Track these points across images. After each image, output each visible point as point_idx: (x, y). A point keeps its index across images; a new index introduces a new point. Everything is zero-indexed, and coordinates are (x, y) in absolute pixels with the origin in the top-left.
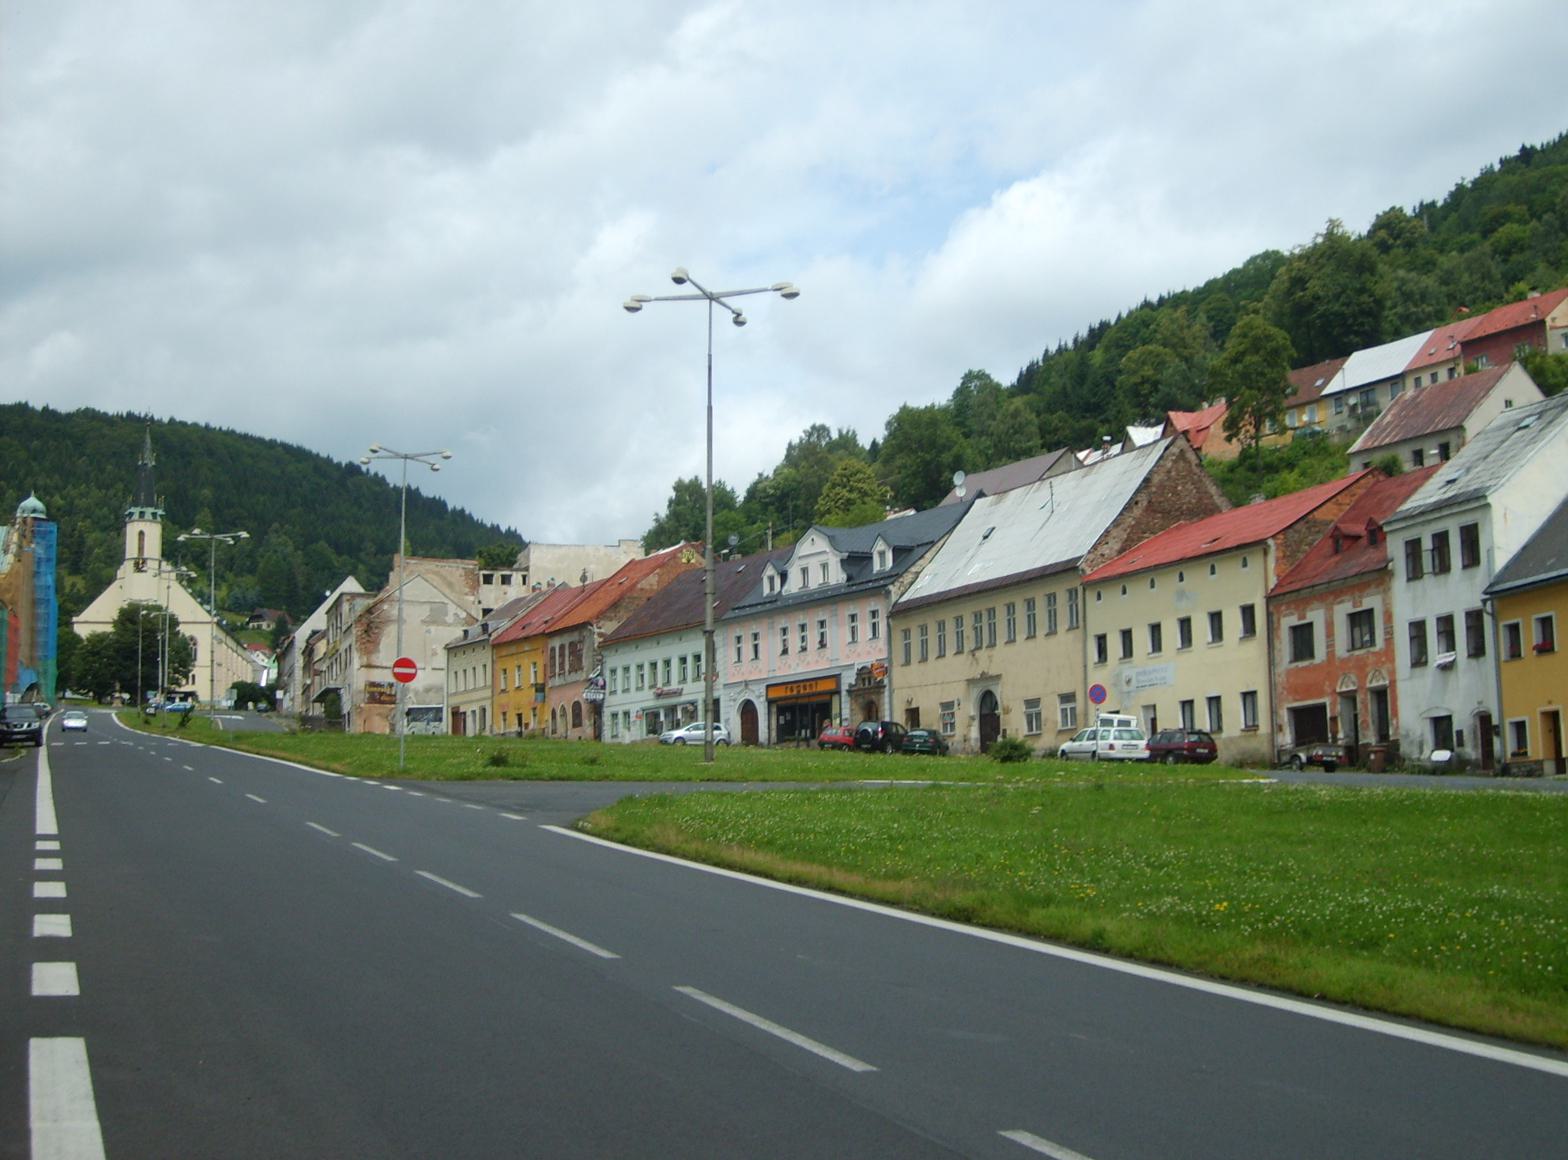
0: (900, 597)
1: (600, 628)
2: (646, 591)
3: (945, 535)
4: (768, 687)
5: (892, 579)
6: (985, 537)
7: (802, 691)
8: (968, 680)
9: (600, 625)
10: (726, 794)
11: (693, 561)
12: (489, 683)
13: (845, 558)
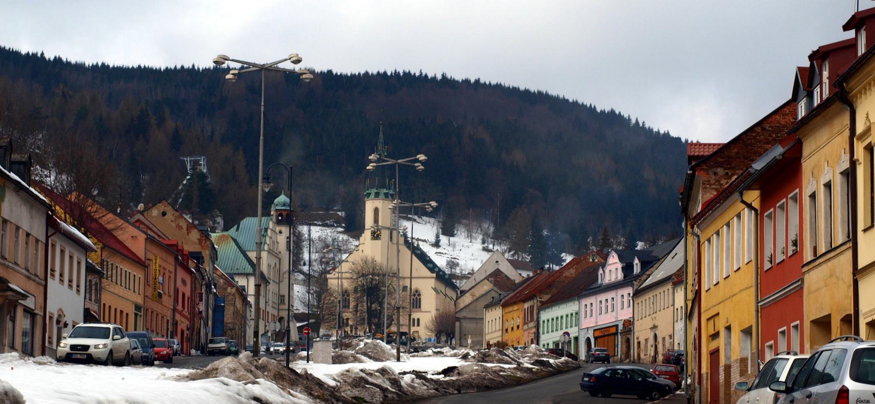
0: (639, 287)
1: (541, 298)
2: (568, 277)
3: (666, 255)
4: (594, 330)
5: (635, 279)
6: (673, 258)
7: (605, 333)
8: (650, 328)
9: (541, 297)
10: (240, 363)
11: (596, 260)
12: (501, 328)
13: (624, 266)
